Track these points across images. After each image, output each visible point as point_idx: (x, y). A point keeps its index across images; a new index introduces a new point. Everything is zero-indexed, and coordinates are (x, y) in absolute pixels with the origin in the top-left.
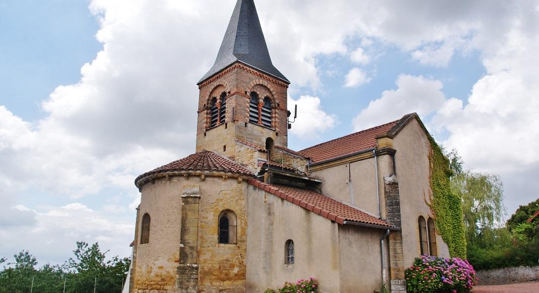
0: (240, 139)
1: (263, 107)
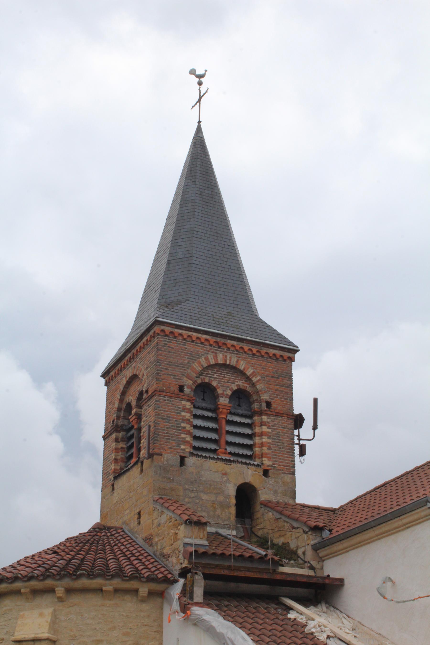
0: (164, 499)
1: (231, 413)
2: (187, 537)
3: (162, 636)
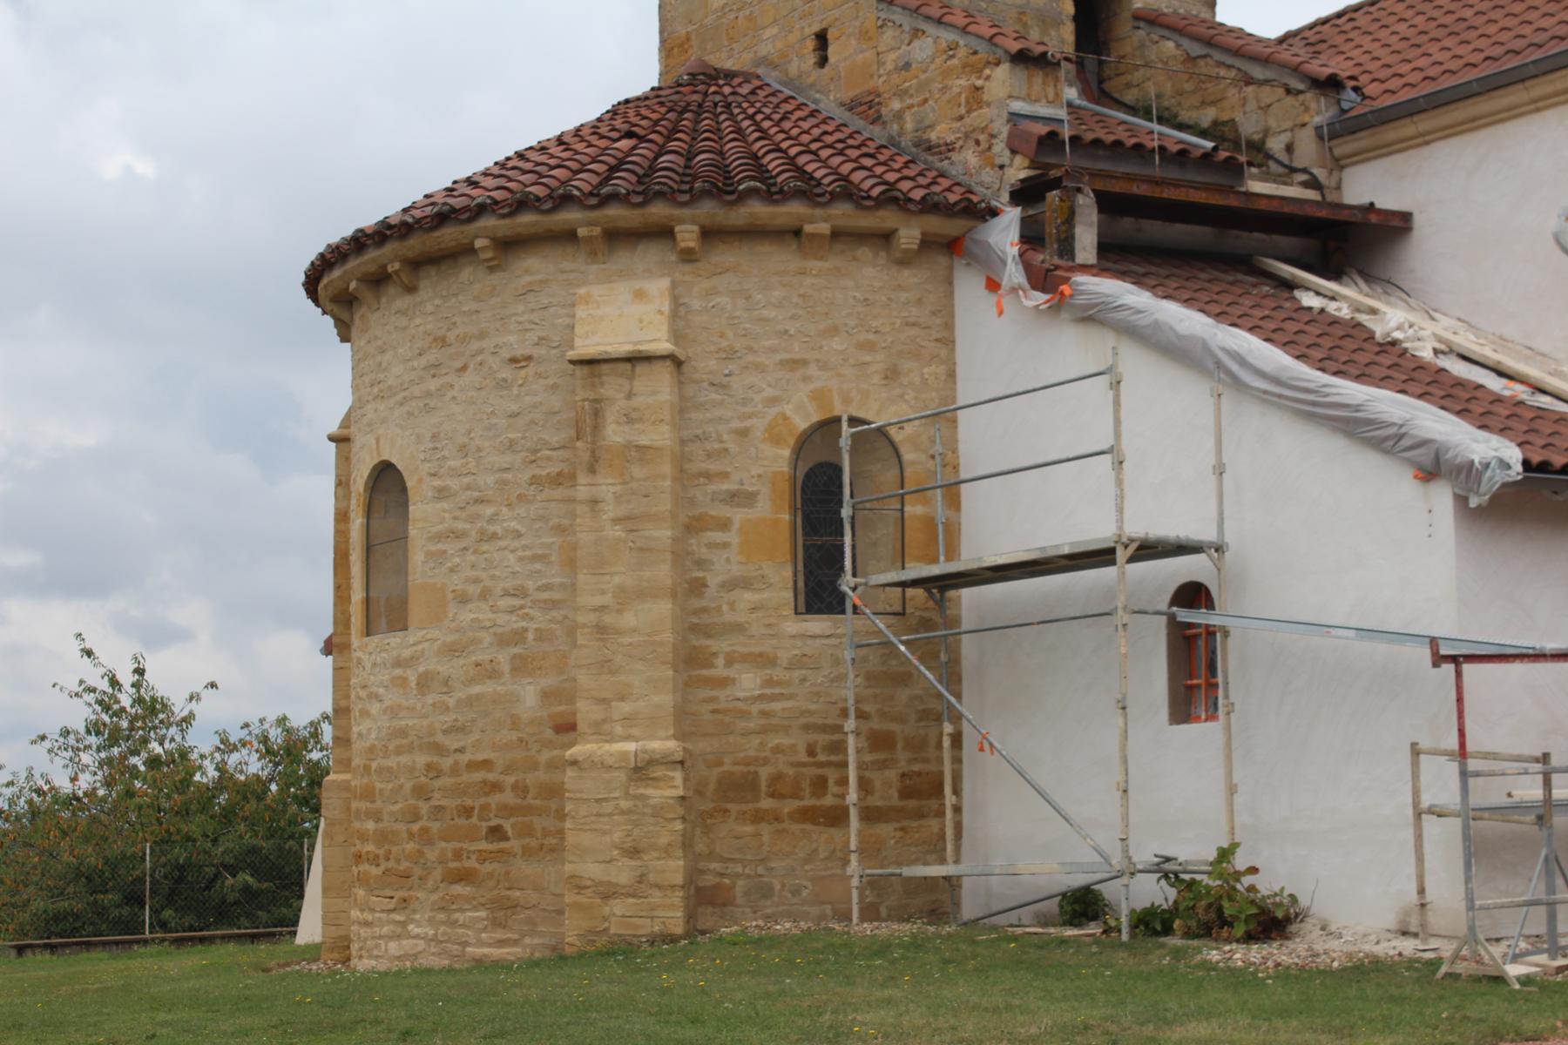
2: (1018, 98)
3: (953, 350)
